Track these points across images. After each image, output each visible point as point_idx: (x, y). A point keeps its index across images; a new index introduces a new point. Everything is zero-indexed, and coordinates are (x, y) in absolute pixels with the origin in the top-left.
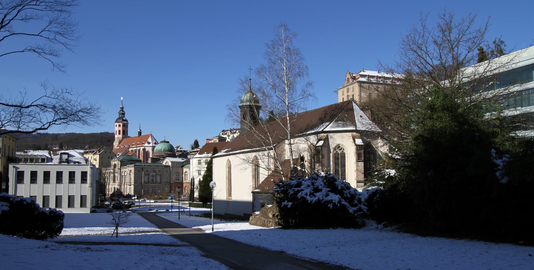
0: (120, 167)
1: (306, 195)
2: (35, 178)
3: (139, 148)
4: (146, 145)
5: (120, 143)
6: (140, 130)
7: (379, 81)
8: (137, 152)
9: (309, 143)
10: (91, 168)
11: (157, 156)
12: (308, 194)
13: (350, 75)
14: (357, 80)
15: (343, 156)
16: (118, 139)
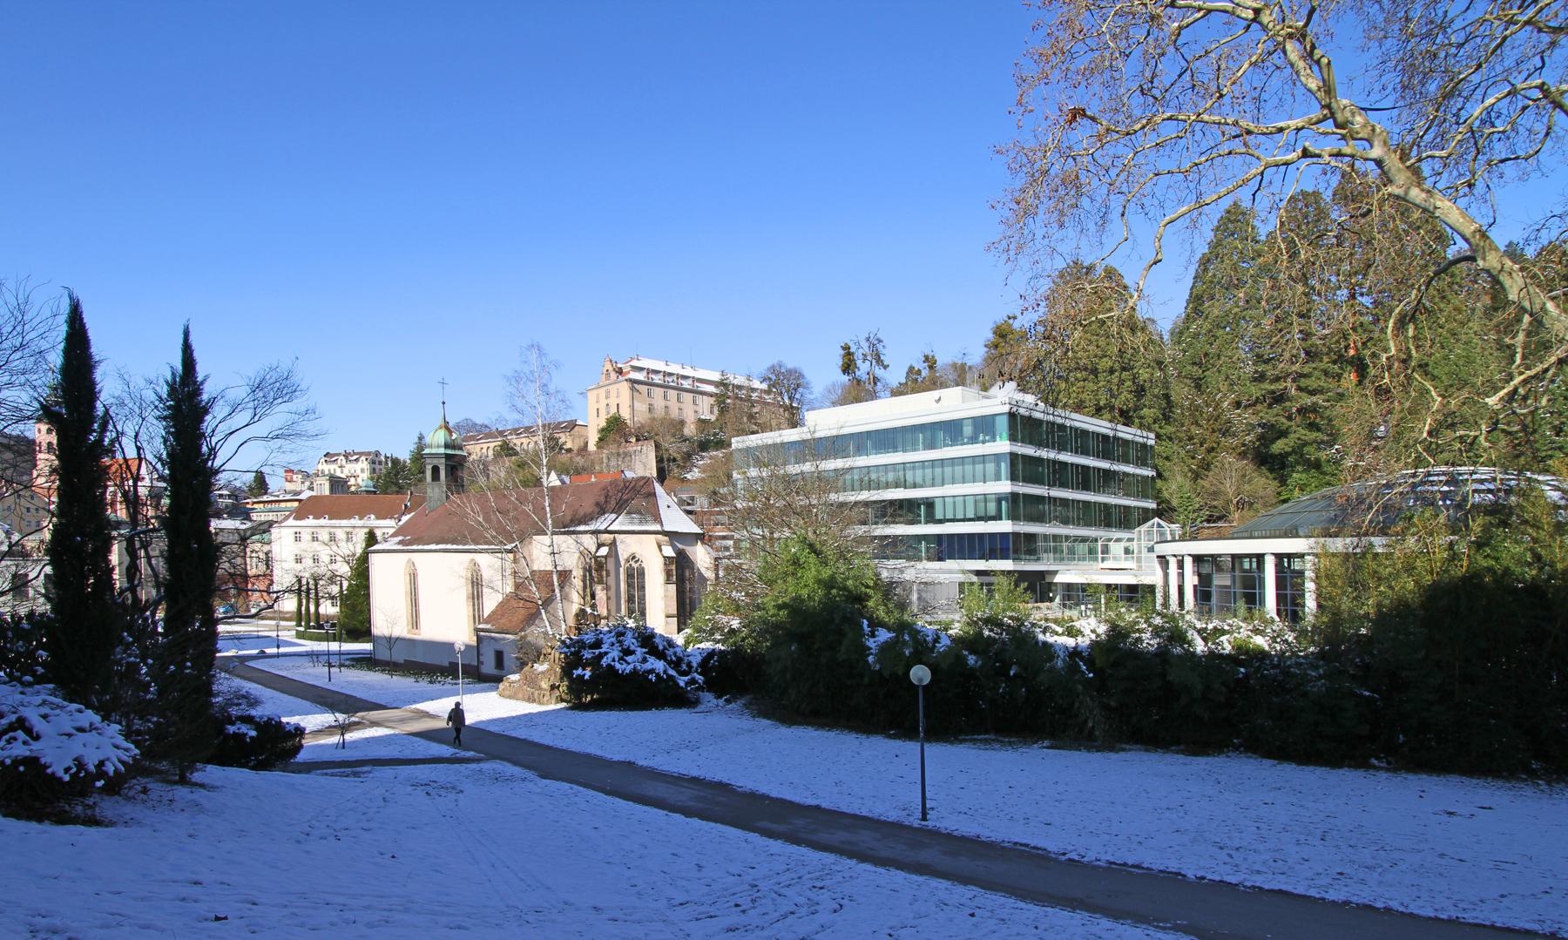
1: (614, 660)
9: (582, 548)
12: (617, 659)
14: (627, 377)
15: (641, 573)
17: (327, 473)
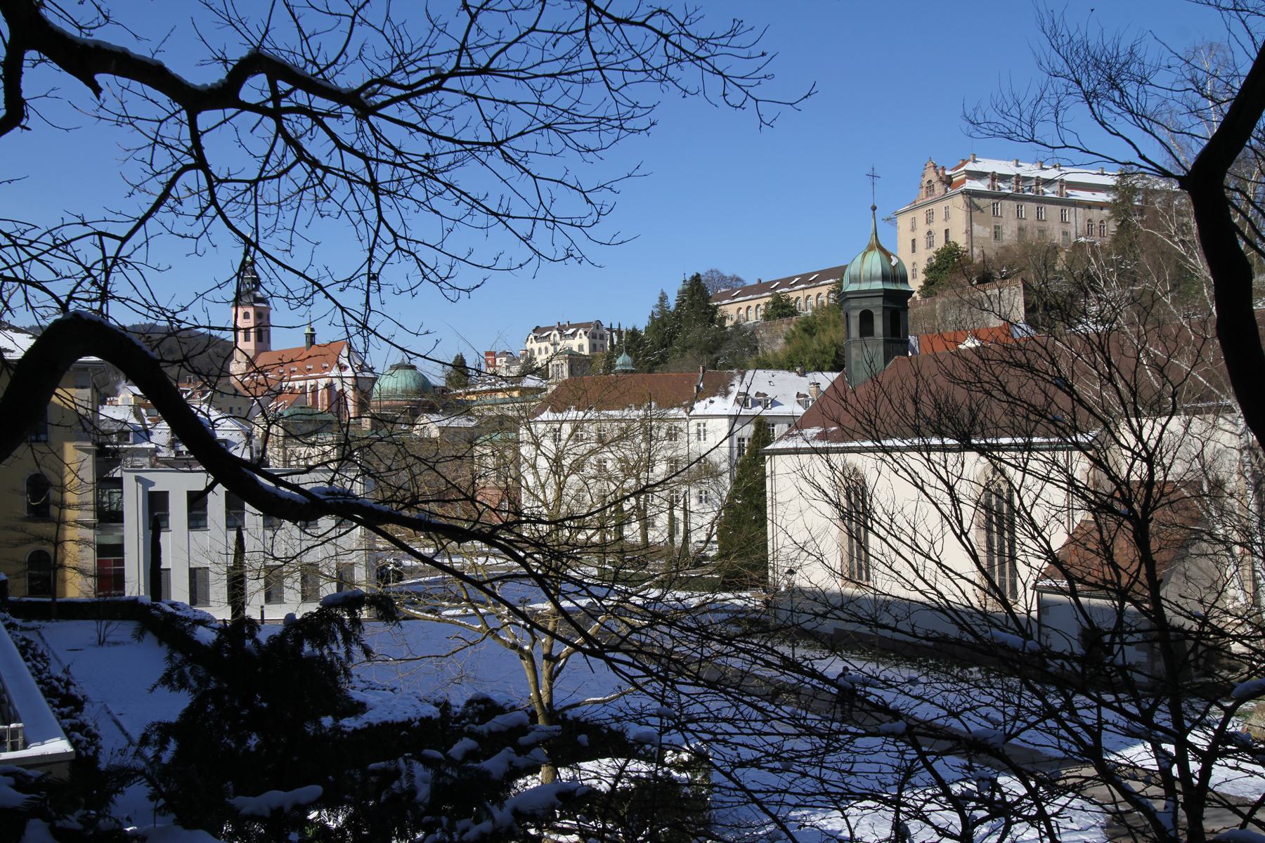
3: (313, 382)
6: (312, 330)
7: (1000, 188)
13: (937, 173)
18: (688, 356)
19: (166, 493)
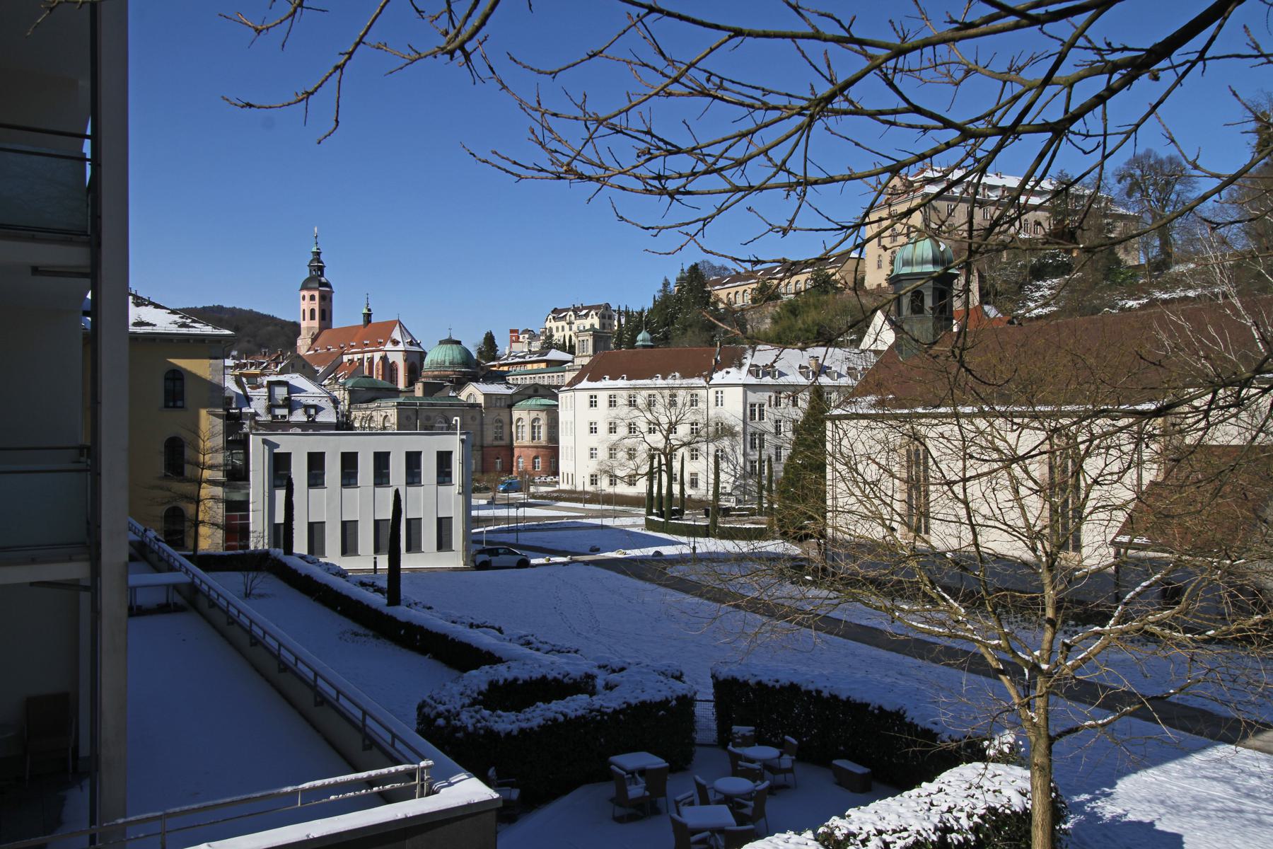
0: (349, 405)
2: (320, 472)
3: (369, 355)
4: (389, 346)
5: (314, 340)
6: (369, 310)
7: (989, 196)
8: (366, 364)
10: (462, 441)
11: (435, 377)
16: (308, 332)
17: (588, 327)
18: (690, 333)
19: (289, 454)
